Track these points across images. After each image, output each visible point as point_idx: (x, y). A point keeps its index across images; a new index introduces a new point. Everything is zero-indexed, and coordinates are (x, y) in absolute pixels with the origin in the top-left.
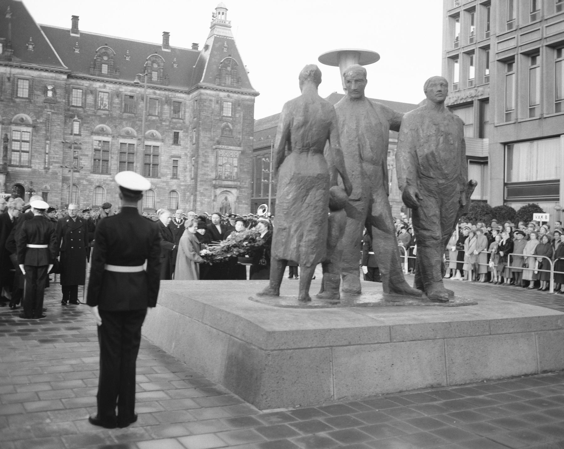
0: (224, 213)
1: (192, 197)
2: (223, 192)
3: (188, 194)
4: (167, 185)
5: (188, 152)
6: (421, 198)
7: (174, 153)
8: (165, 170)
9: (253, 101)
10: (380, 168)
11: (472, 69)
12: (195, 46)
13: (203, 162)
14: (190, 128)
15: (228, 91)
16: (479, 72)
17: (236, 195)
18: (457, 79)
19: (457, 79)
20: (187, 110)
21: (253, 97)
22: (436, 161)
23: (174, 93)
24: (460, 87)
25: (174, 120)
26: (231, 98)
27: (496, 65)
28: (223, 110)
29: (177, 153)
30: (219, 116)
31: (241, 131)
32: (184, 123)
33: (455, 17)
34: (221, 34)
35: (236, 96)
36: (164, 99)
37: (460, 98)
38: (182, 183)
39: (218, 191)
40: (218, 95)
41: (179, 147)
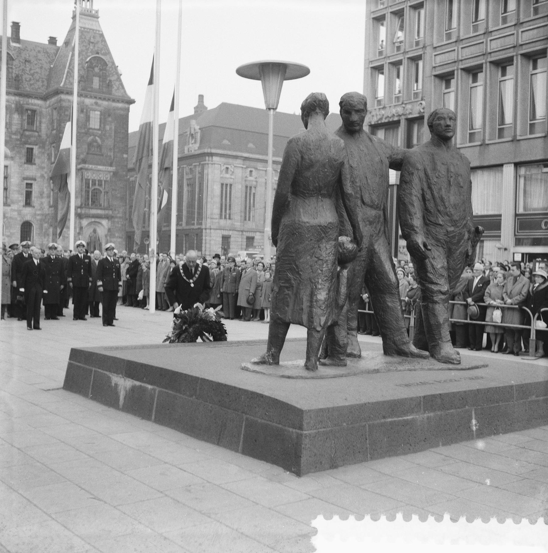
0: (92, 249)
1: (51, 230)
2: (90, 224)
3: (46, 225)
5: (46, 173)
6: (429, 247)
9: (128, 110)
10: (381, 213)
11: (398, 83)
12: (53, 40)
15: (96, 98)
16: (408, 85)
17: (106, 227)
18: (381, 94)
19: (381, 94)
21: (127, 106)
23: (26, 100)
24: (385, 103)
25: (27, 133)
26: (99, 106)
27: (433, 81)
28: (89, 120)
29: (31, 174)
31: (112, 146)
32: (40, 136)
33: (379, 19)
34: (87, 26)
35: (105, 103)
36: (13, 106)
37: (384, 117)
38: (38, 212)
39: (85, 222)
40: (83, 103)
41: (34, 167)
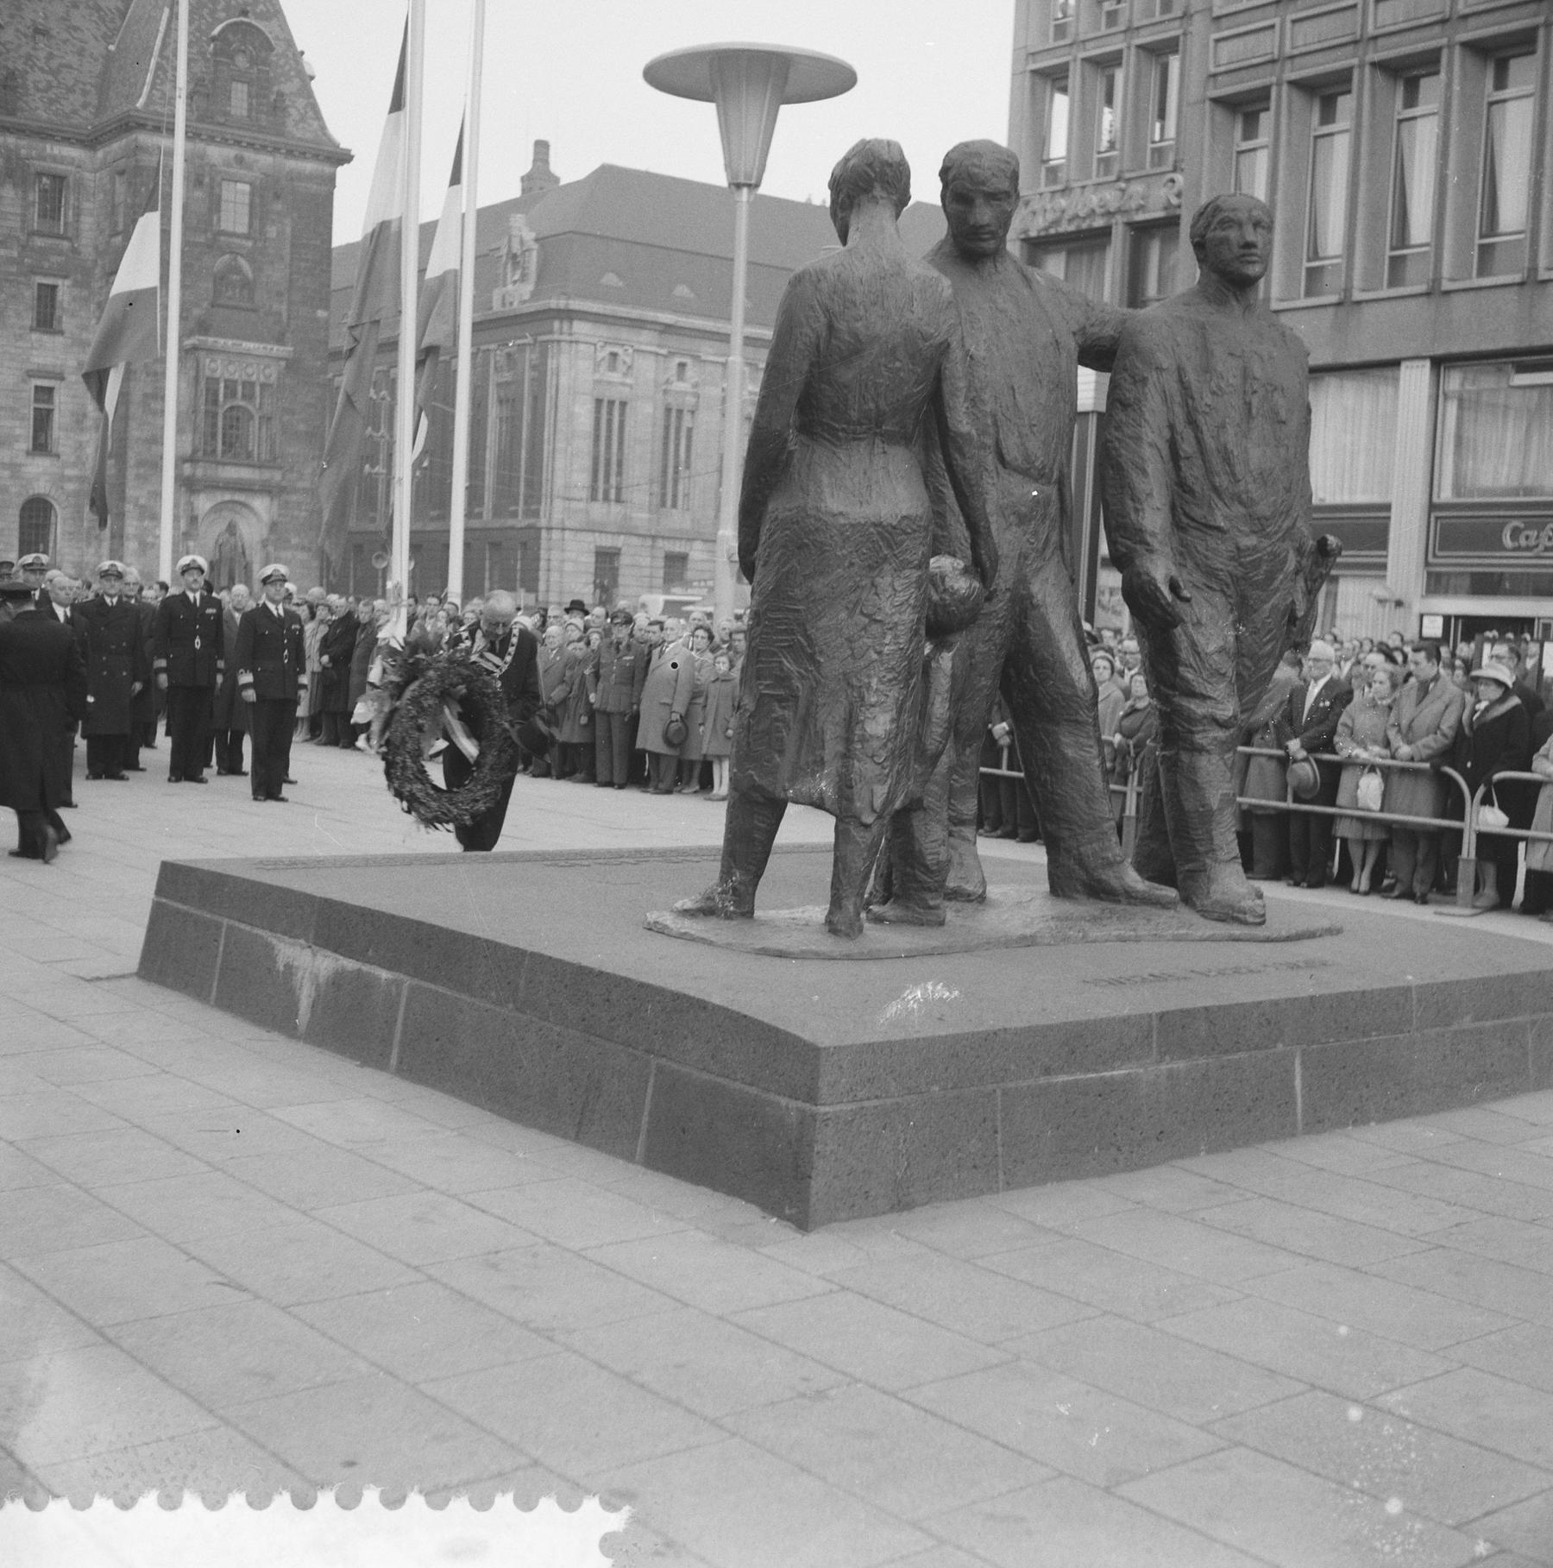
2: (218, 508)
4: (12, 477)
6: (1186, 593)
7: (40, 360)
8: (8, 423)
11: (1109, 119)
13: (146, 395)
14: (98, 271)
15: (238, 143)
17: (265, 517)
20: (87, 205)
21: (327, 169)
22: (1233, 474)
23: (37, 144)
25: (39, 242)
26: (250, 168)
30: (205, 232)
32: (75, 251)
35: (265, 160)
38: (69, 472)
39: (204, 503)
41: (59, 339)
